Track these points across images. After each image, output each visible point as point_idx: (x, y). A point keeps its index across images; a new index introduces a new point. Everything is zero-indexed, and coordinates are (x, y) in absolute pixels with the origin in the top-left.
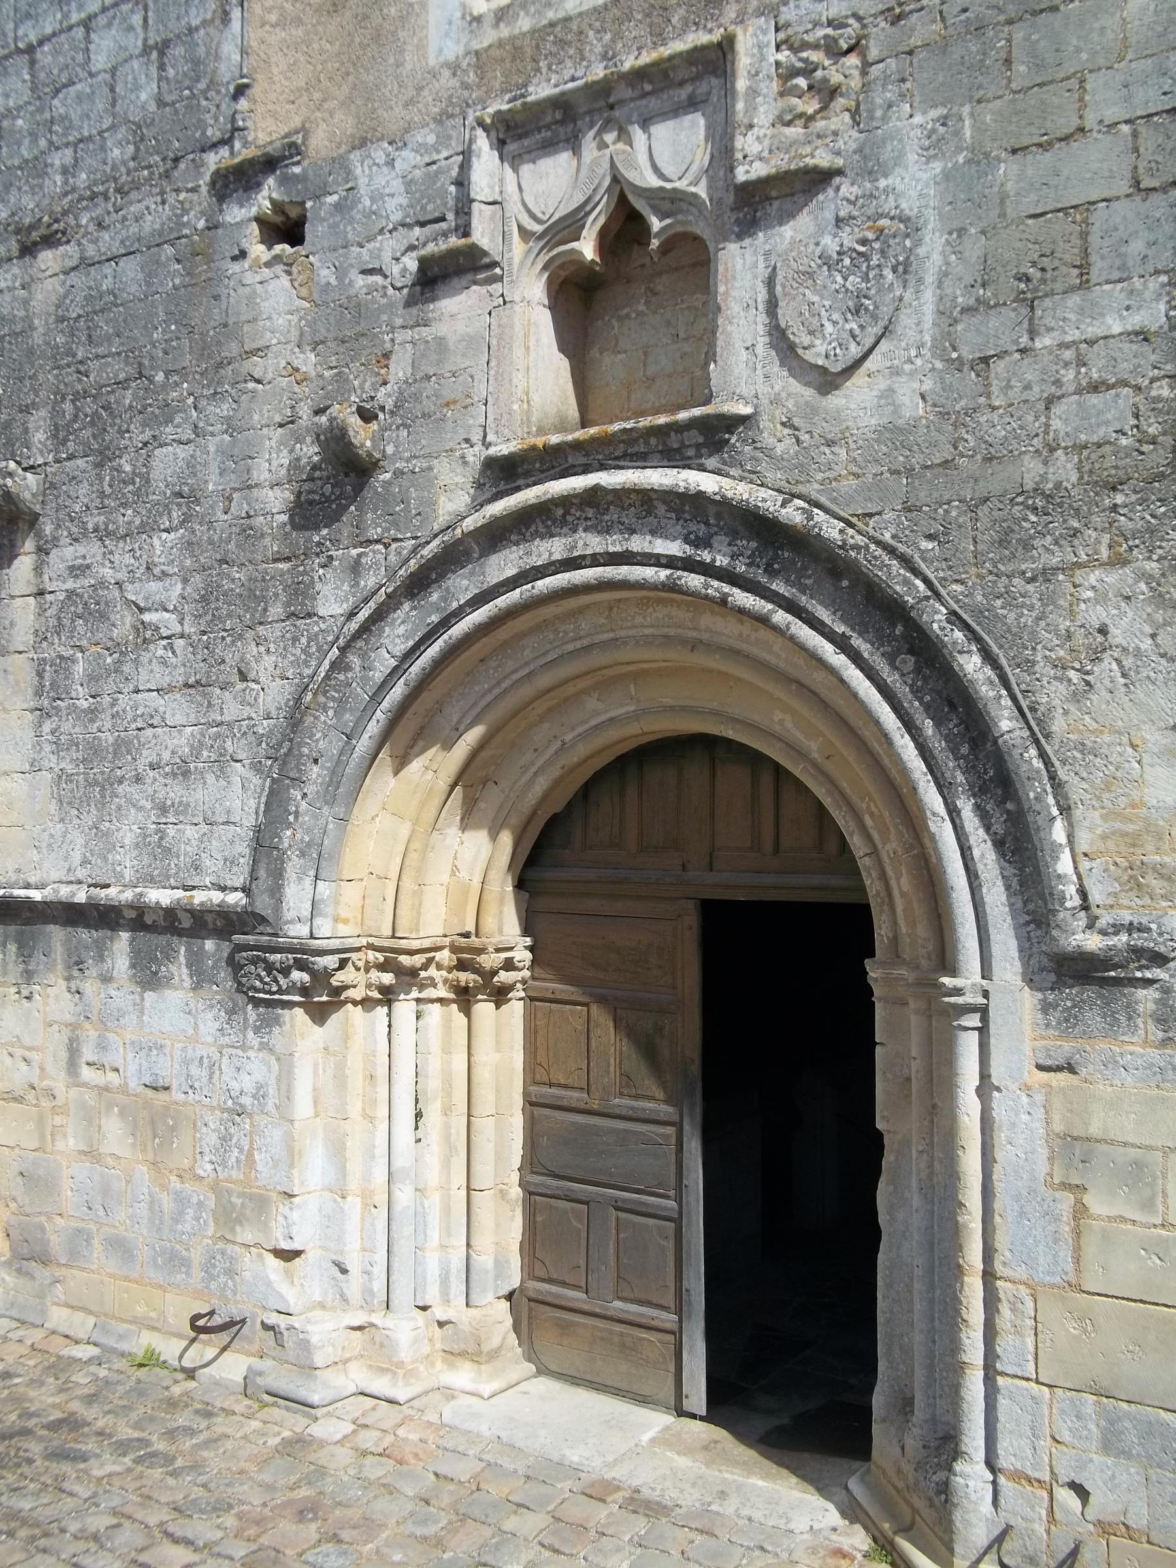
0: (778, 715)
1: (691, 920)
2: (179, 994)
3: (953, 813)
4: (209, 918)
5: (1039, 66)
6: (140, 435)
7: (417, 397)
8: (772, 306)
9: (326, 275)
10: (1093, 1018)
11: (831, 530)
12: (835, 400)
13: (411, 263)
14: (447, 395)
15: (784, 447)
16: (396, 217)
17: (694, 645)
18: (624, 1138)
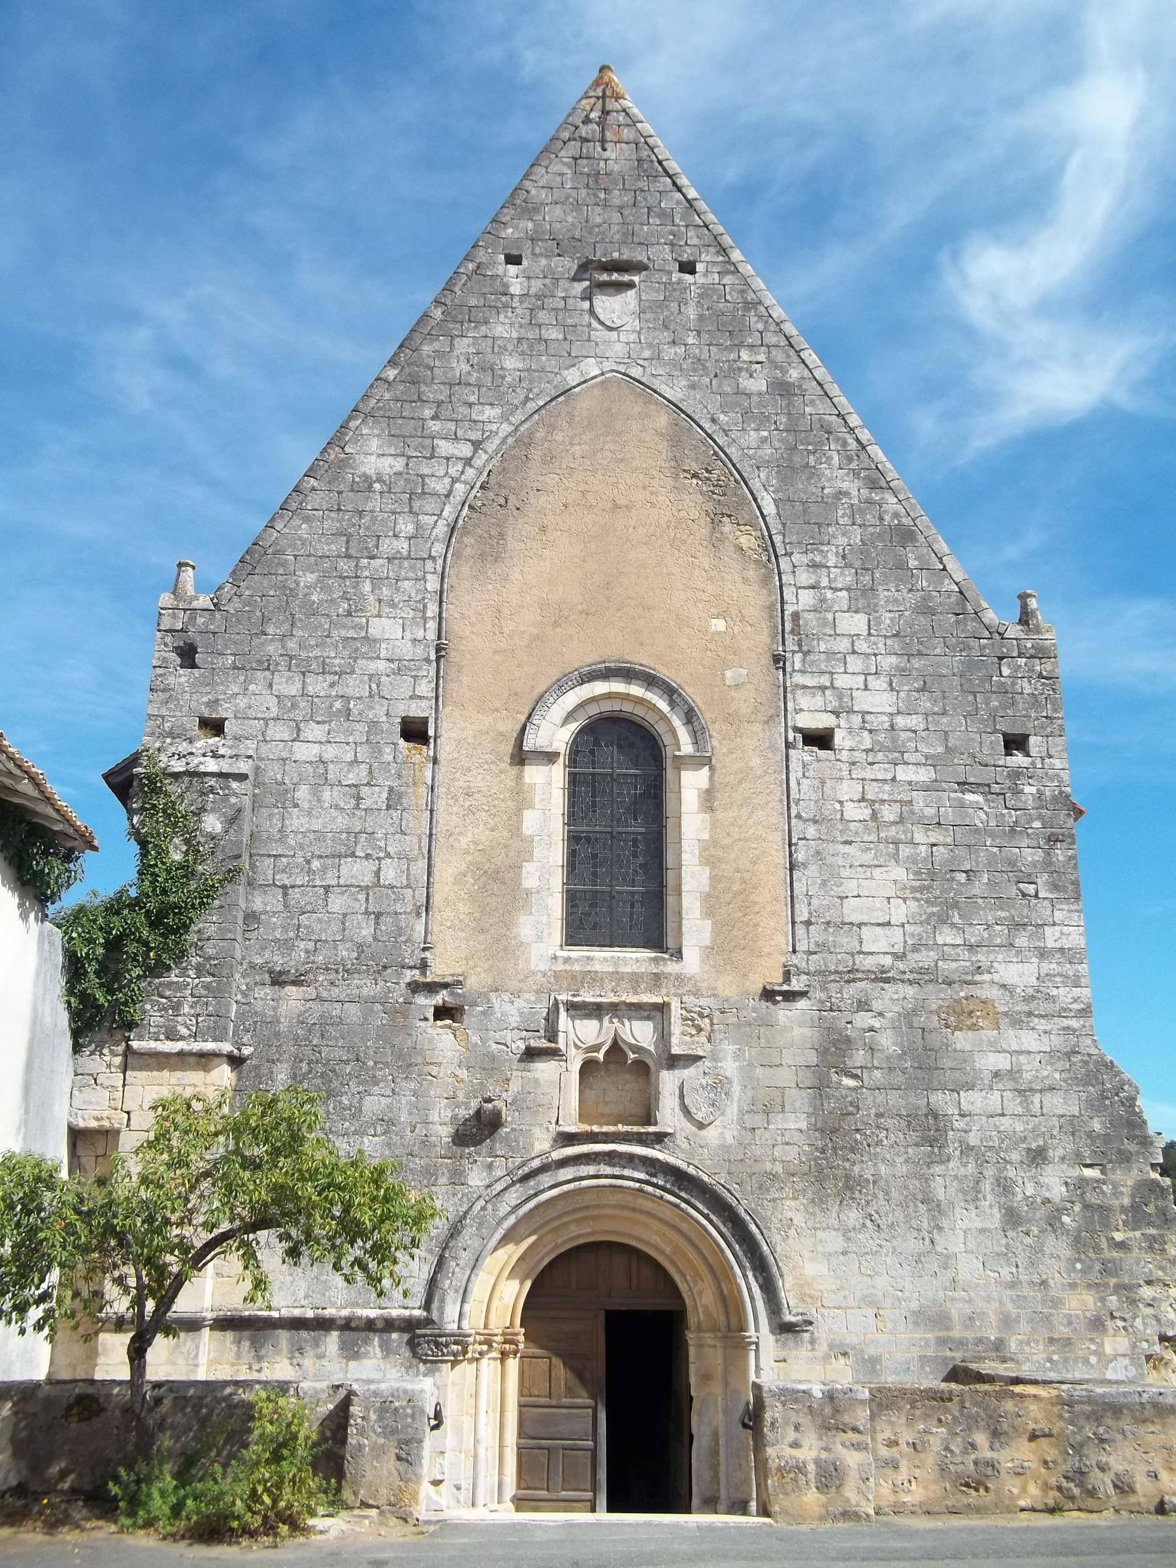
0: (654, 1237)
1: (602, 1318)
2: (374, 1361)
3: (745, 1276)
4: (397, 1323)
5: (768, 1042)
6: (354, 1087)
7: (524, 1100)
8: (682, 1096)
9: (475, 1039)
10: (791, 1344)
11: (705, 1178)
12: (703, 1133)
13: (522, 1046)
14: (539, 1101)
15: (685, 1145)
16: (515, 1025)
17: (634, 1210)
18: (568, 1416)
